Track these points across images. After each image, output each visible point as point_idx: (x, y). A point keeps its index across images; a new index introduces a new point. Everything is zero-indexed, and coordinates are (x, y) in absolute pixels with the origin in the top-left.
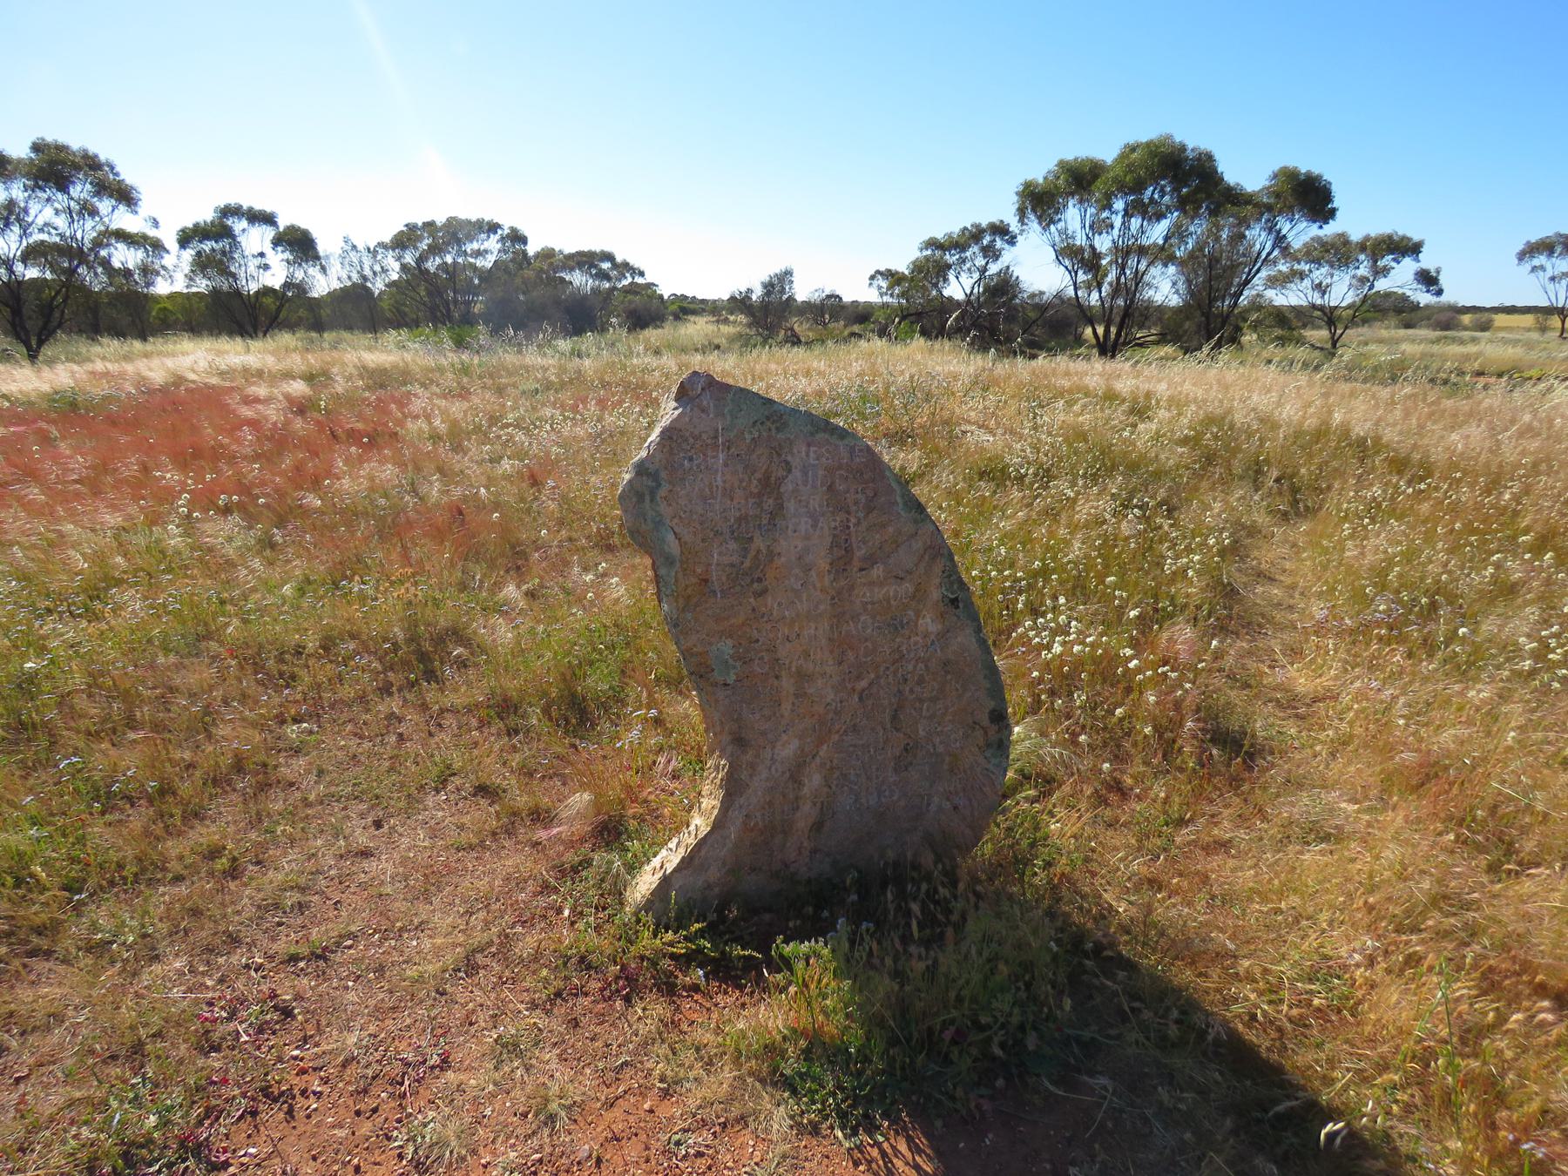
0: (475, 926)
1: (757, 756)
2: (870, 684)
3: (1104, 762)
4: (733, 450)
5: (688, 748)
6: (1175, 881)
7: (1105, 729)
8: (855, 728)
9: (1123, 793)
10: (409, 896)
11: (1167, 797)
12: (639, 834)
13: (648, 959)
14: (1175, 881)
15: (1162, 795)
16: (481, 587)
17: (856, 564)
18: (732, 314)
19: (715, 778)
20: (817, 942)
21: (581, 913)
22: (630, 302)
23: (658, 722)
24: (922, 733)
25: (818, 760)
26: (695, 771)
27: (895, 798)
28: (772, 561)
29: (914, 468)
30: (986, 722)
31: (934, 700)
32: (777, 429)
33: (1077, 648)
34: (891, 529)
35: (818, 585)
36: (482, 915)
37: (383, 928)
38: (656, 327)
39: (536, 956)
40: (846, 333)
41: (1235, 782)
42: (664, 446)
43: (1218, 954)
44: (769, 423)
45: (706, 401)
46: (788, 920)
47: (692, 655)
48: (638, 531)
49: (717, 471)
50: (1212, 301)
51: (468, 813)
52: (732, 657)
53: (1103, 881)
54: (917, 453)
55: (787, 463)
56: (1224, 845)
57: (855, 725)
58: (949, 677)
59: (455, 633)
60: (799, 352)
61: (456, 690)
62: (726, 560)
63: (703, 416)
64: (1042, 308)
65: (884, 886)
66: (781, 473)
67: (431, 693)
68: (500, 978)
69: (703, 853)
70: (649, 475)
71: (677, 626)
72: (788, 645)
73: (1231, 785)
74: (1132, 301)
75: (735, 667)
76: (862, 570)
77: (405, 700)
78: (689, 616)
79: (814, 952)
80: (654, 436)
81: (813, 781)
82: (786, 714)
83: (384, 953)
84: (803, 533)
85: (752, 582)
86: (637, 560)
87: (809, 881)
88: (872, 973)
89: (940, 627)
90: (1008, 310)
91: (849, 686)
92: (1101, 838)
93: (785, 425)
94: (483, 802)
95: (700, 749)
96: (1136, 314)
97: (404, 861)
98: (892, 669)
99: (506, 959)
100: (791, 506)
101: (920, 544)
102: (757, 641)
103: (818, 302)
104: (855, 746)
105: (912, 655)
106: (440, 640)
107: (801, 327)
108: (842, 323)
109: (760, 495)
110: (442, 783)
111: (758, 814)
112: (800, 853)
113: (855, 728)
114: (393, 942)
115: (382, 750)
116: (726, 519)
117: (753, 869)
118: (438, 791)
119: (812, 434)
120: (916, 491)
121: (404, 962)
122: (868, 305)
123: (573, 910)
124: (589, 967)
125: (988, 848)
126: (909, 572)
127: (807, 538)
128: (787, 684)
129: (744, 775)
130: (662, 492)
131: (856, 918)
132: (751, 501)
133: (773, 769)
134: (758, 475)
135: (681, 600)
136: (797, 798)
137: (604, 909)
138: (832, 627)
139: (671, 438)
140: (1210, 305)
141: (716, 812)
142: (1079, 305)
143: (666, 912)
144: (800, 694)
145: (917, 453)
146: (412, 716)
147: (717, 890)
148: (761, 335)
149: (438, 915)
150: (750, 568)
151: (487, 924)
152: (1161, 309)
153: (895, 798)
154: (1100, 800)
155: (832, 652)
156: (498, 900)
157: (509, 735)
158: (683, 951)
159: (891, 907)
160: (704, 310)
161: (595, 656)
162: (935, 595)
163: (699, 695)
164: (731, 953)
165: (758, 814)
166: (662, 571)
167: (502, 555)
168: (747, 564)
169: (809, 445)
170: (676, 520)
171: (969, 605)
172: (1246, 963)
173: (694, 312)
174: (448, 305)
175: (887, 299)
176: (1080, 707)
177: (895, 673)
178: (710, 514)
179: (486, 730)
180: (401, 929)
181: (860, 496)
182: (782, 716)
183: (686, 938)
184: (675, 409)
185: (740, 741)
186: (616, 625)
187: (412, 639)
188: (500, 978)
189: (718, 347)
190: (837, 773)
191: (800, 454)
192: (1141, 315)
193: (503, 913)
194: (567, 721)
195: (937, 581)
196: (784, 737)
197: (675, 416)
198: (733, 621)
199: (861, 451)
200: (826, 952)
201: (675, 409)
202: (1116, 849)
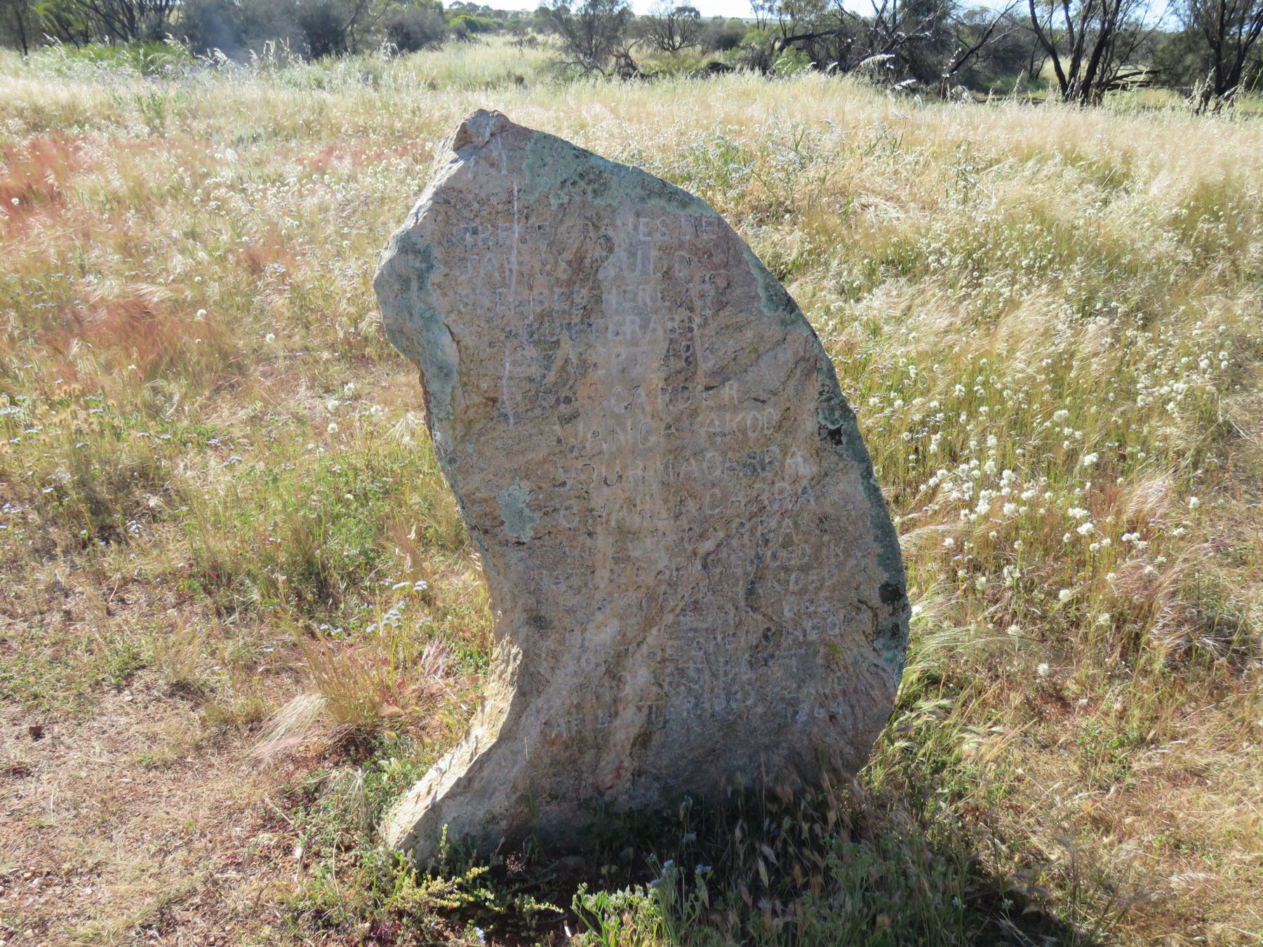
0: (171, 870)
1: (561, 642)
2: (718, 546)
3: (1040, 661)
4: (531, 221)
5: (467, 635)
6: (1128, 820)
7: (1043, 618)
8: (696, 606)
9: (1065, 704)
10: (81, 829)
11: (1125, 709)
12: (398, 749)
13: (410, 915)
14: (1128, 820)
15: (1118, 706)
16: (179, 410)
17: (701, 380)
18: (540, 31)
19: (503, 672)
20: (633, 891)
21: (317, 854)
22: (395, 12)
23: (427, 599)
24: (788, 614)
25: (644, 648)
26: (478, 667)
27: (750, 702)
28: (584, 375)
29: (792, 256)
30: (876, 600)
31: (805, 569)
32: (594, 191)
33: (1008, 508)
34: (749, 334)
35: (648, 409)
36: (181, 854)
37: (46, 870)
38: (433, 48)
39: (256, 910)
40: (705, 62)
41: (1218, 692)
42: (438, 212)
43: (1181, 916)
44: (582, 184)
45: (497, 150)
46: (600, 865)
47: (474, 502)
48: (401, 332)
49: (511, 248)
50: (1224, 25)
51: (161, 719)
52: (528, 506)
53: (1032, 820)
54: (798, 234)
55: (608, 239)
56: (1198, 775)
57: (696, 602)
58: (826, 538)
59: (144, 474)
60: (633, 90)
61: (144, 553)
62: (522, 372)
63: (493, 172)
64: (985, 32)
65: (732, 822)
66: (599, 253)
67: (110, 559)
68: (206, 937)
69: (485, 773)
70: (416, 252)
71: (450, 459)
72: (605, 490)
73: (1211, 694)
74: (1112, 23)
75: (532, 520)
76: (708, 388)
77: (73, 566)
78: (470, 448)
79: (631, 906)
80: (425, 199)
81: (638, 677)
82: (602, 586)
83: (46, 903)
84: (628, 337)
85: (558, 401)
86: (402, 379)
87: (630, 814)
88: (707, 930)
89: (815, 469)
90: (937, 32)
91: (690, 548)
92: (1032, 763)
93: (605, 186)
94: (184, 706)
95: (484, 637)
96: (1118, 43)
97: (74, 781)
98: (748, 526)
99: (214, 913)
100: (612, 299)
101: (789, 354)
102: (564, 484)
103: (664, 17)
104: (695, 630)
105: (776, 507)
106: (121, 485)
107: (640, 53)
108: (699, 48)
109: (570, 283)
110: (126, 677)
111: (562, 721)
112: (618, 776)
113: (696, 606)
114: (58, 890)
115: (41, 634)
116: (523, 316)
117: (553, 797)
118: (119, 689)
119: (643, 199)
120: (793, 290)
121: (76, 915)
122: (737, 23)
123: (308, 847)
124: (328, 925)
125: (879, 774)
126: (774, 393)
127: (634, 343)
128: (604, 544)
129: (544, 668)
130: (435, 277)
131: (687, 862)
132: (558, 290)
133: (583, 660)
134: (568, 255)
135: (459, 426)
136: (615, 701)
137: (348, 849)
138: (666, 467)
139: (447, 202)
140: (1222, 32)
141: (504, 717)
142: (1037, 29)
143: (434, 853)
144: (621, 559)
145: (798, 234)
146: (84, 588)
147: (504, 824)
148: (581, 63)
149: (120, 853)
150: (555, 384)
151: (188, 865)
152: (1152, 36)
153: (750, 702)
154: (1033, 711)
155: (666, 501)
156: (203, 835)
157: (219, 615)
158: (457, 904)
159: (741, 850)
160: (501, 26)
161: (339, 508)
162: (809, 424)
163: (484, 558)
164: (521, 907)
165: (562, 721)
166: (434, 386)
167: (209, 368)
168: (551, 377)
169: (638, 215)
170: (453, 316)
171: (856, 440)
172: (1218, 927)
173: (485, 29)
174: (131, 11)
175: (764, 15)
176: (1011, 588)
177: (752, 531)
178: (499, 309)
179: (187, 608)
180: (69, 873)
181: (707, 286)
182: (597, 588)
183: (461, 888)
184: (453, 162)
185: (538, 622)
186: (369, 466)
187: (82, 484)
188: (206, 937)
189: (520, 80)
190: (670, 668)
191: (624, 227)
192: (1125, 44)
193: (209, 852)
194: (300, 596)
195: (812, 406)
196: (599, 617)
197: (453, 171)
198: (530, 456)
199: (709, 224)
200: (646, 903)
201: (453, 162)
202: (1051, 777)
